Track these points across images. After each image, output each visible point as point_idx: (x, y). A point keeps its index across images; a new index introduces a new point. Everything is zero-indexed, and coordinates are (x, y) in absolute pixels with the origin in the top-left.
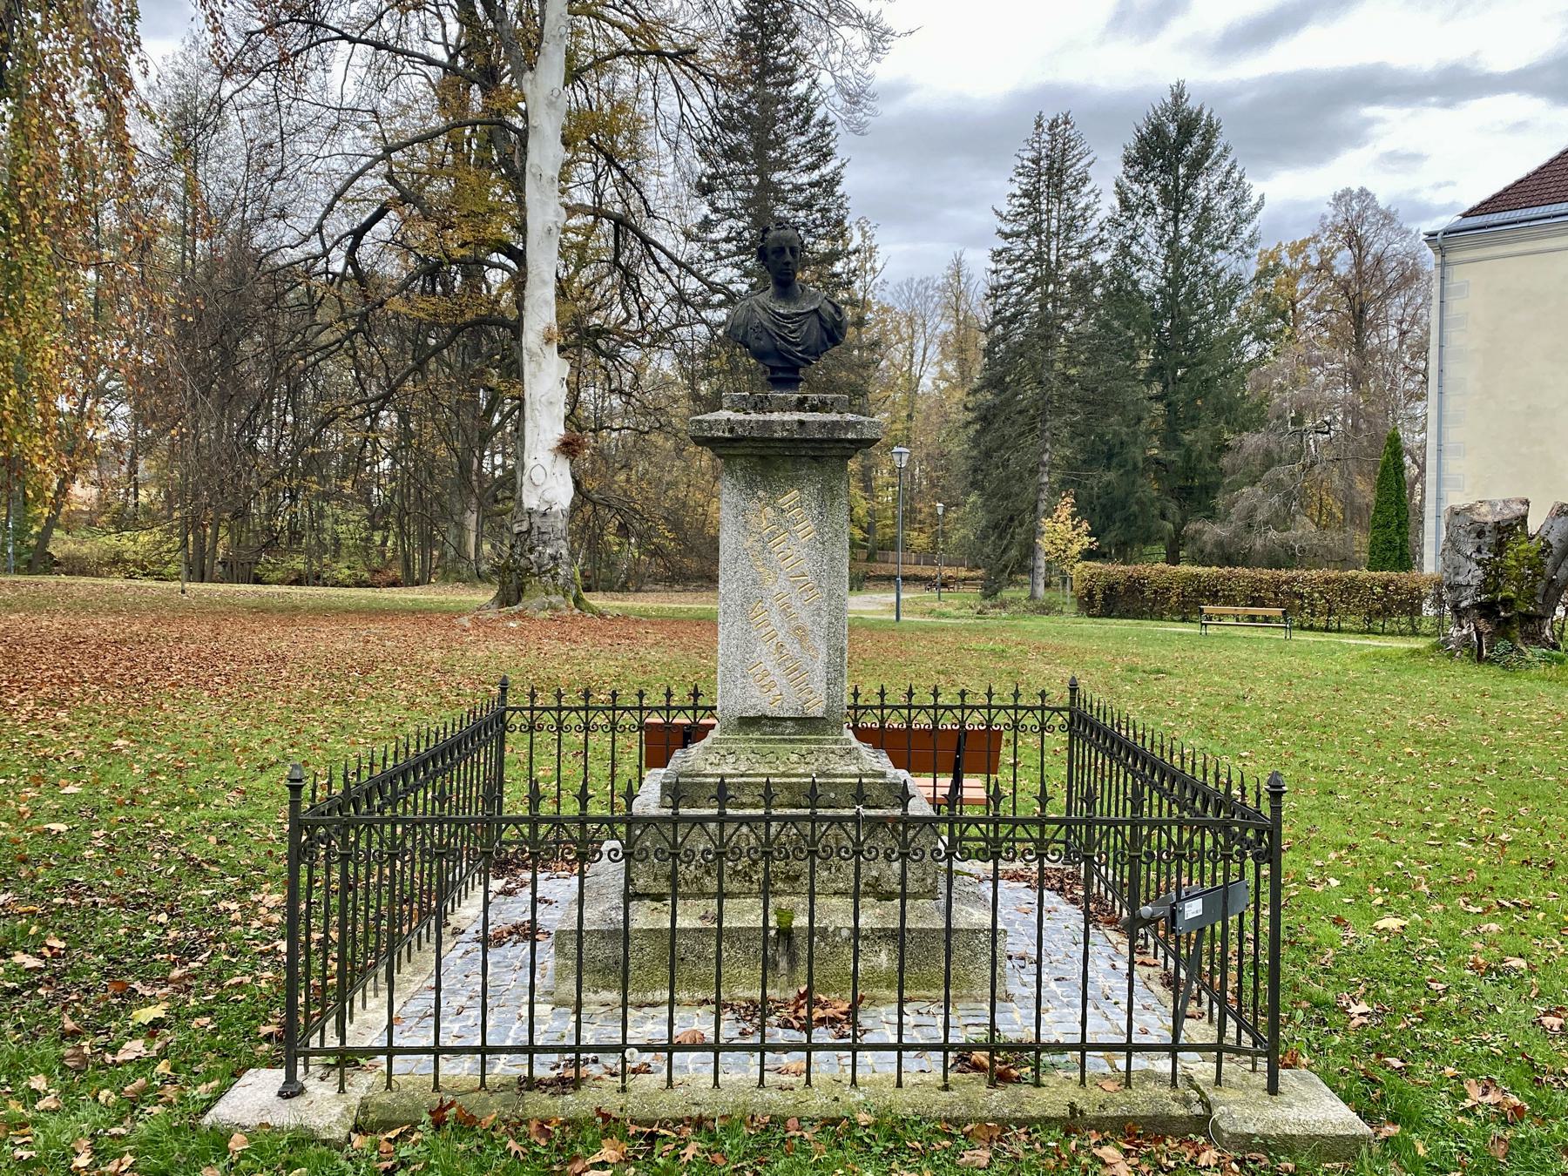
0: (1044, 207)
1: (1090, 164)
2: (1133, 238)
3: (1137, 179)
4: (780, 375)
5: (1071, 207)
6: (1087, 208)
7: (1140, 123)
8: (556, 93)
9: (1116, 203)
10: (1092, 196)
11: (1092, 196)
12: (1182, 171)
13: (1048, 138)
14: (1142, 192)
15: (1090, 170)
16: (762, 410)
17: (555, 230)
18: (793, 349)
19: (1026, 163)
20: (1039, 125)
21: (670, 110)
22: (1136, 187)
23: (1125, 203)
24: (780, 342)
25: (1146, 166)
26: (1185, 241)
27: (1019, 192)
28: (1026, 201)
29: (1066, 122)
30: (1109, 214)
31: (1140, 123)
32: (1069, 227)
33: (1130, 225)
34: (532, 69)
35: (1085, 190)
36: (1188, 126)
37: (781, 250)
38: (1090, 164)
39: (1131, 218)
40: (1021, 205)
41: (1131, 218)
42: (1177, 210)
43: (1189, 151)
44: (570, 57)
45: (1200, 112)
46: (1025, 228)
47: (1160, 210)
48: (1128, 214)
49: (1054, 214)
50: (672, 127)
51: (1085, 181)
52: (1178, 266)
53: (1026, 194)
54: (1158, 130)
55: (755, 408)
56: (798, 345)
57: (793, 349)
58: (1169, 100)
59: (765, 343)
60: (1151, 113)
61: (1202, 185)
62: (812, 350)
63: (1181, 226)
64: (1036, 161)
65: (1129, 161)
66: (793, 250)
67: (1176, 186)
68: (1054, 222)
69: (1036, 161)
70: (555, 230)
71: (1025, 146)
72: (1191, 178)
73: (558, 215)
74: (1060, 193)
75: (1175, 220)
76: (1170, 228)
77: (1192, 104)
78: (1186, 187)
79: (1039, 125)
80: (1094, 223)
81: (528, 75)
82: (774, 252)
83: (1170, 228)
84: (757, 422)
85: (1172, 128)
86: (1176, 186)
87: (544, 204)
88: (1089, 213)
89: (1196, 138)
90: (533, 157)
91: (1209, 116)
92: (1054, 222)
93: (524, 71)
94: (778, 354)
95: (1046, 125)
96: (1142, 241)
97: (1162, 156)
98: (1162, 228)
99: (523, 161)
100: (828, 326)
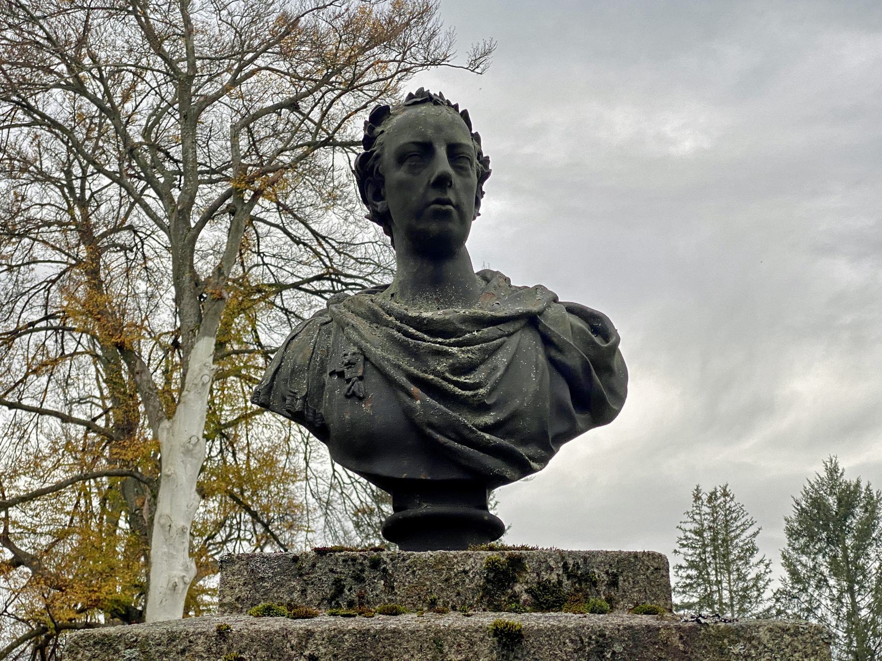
0: (713, 578)
1: (755, 535)
2: (809, 610)
3: (803, 551)
4: (426, 508)
5: (742, 578)
6: (758, 578)
7: (799, 496)
8: (194, 440)
9: (786, 575)
10: (762, 567)
11: (762, 567)
12: (849, 542)
13: (708, 510)
14: (811, 564)
15: (757, 541)
16: (359, 606)
17: (181, 586)
18: (468, 420)
19: (689, 534)
20: (697, 498)
21: (320, 468)
22: (804, 559)
23: (794, 573)
24: (420, 401)
25: (811, 537)
26: (864, 613)
27: (685, 564)
28: (693, 572)
29: (725, 494)
30: (781, 586)
31: (799, 496)
32: (744, 598)
33: (804, 597)
34: (169, 418)
35: (753, 560)
36: (848, 498)
37: (425, 150)
38: (755, 535)
39: (805, 590)
40: (688, 577)
41: (805, 590)
42: (851, 581)
43: (853, 522)
44: (212, 413)
45: (858, 485)
46: (695, 600)
47: (832, 582)
48: (800, 586)
49: (725, 585)
50: (323, 487)
51: (753, 550)
52: (862, 640)
53: (692, 565)
54: (817, 503)
55: (334, 600)
56: (482, 408)
57: (468, 420)
58: (824, 474)
59: (376, 409)
60: (808, 487)
61: (873, 555)
62: (528, 425)
63: (859, 598)
64: (699, 533)
65: (792, 533)
66: (455, 152)
67: (846, 556)
68: (726, 594)
69: (699, 533)
70: (181, 586)
71: (686, 518)
72: (861, 549)
73: (186, 569)
74: (728, 564)
75: (851, 590)
76: (847, 599)
77: (849, 478)
78: (857, 558)
79: (697, 498)
80: (768, 594)
81: (166, 424)
82: (402, 157)
83: (847, 599)
84: (334, 638)
85: (832, 501)
86: (846, 556)
87: (171, 556)
88: (761, 583)
89: (858, 510)
90: (164, 507)
91: (868, 489)
92: (726, 594)
93: (160, 420)
94: (418, 438)
95: (705, 497)
96: (819, 613)
97: (825, 527)
98: (839, 600)
99: (152, 512)
100: (573, 360)
